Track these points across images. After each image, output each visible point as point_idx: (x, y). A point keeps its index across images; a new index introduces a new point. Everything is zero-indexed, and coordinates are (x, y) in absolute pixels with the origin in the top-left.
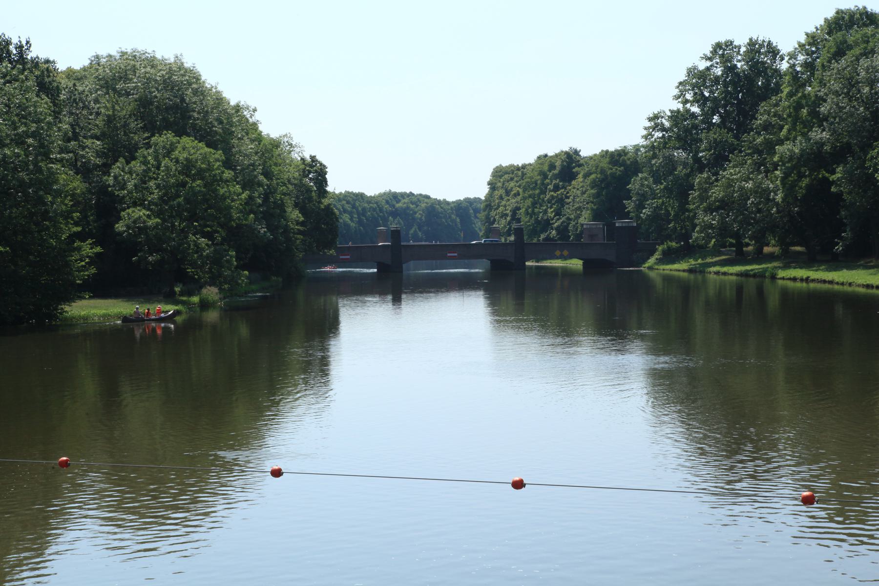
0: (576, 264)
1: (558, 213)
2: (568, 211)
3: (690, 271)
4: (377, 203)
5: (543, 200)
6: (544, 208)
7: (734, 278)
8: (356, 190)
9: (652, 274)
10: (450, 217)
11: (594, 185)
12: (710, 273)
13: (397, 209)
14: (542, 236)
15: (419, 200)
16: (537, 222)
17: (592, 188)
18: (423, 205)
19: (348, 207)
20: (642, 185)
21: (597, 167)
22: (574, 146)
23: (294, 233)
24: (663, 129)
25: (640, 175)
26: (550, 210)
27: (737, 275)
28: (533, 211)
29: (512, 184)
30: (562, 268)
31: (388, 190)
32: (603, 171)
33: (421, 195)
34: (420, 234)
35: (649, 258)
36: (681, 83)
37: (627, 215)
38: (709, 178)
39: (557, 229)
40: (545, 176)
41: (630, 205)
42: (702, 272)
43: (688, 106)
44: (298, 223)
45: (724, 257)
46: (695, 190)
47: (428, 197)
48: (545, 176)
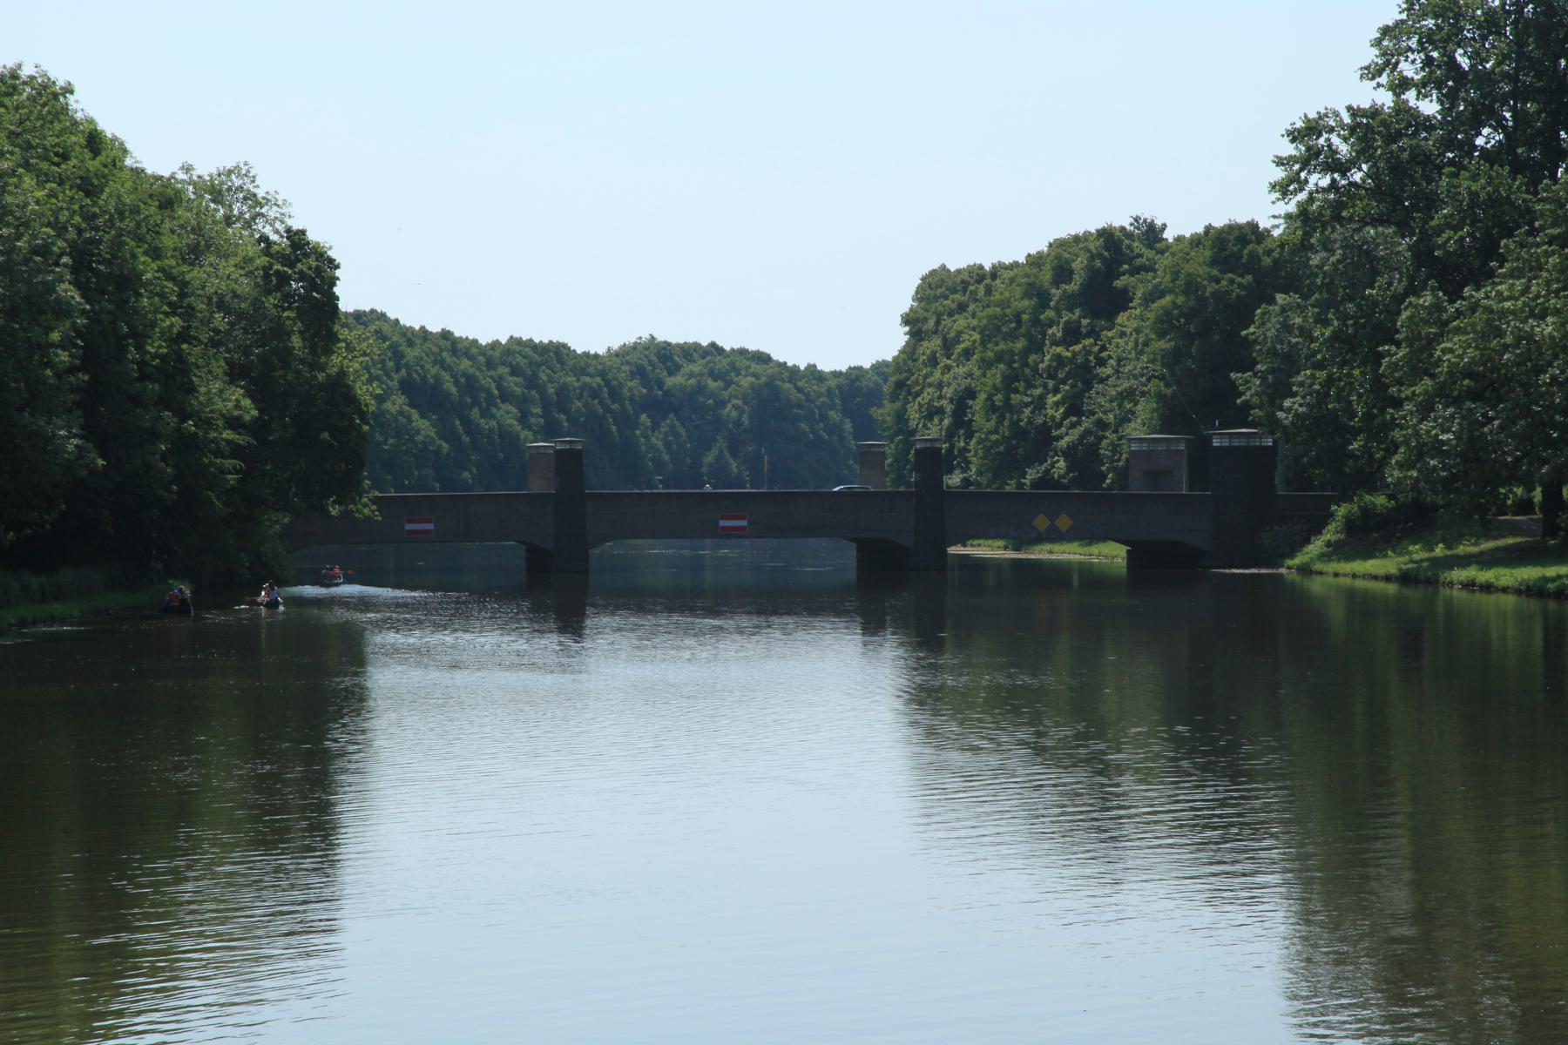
0: (1112, 555)
1: (1075, 408)
2: (1101, 400)
3: (1405, 578)
4: (603, 374)
5: (1035, 369)
6: (1038, 392)
7: (1510, 600)
8: (542, 335)
9: (1316, 586)
10: (824, 417)
11: (1165, 325)
12: (1451, 584)
13: (668, 394)
14: (1031, 475)
15: (734, 368)
16: (1018, 432)
17: (1161, 335)
18: (746, 382)
19: (514, 385)
20: (1286, 328)
21: (1176, 275)
22: (1147, 214)
23: (218, 453)
24: (1336, 165)
25: (1280, 298)
26: (1051, 399)
27: (1518, 591)
28: (1007, 399)
29: (961, 322)
30: (1293, 583)
31: (646, 336)
32: (1192, 287)
33: (743, 352)
34: (734, 465)
35: (1308, 542)
36: (1386, 31)
37: (1240, 416)
38: (1437, 307)
39: (1068, 453)
40: (1043, 299)
41: (1249, 386)
42: (1432, 582)
43: (1410, 96)
44: (234, 423)
45: (1510, 541)
46: (1398, 344)
47: (762, 358)
48: (1043, 299)
